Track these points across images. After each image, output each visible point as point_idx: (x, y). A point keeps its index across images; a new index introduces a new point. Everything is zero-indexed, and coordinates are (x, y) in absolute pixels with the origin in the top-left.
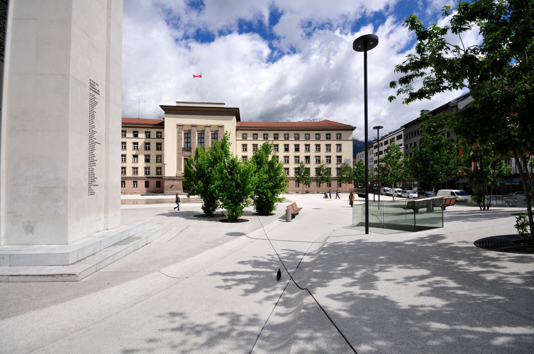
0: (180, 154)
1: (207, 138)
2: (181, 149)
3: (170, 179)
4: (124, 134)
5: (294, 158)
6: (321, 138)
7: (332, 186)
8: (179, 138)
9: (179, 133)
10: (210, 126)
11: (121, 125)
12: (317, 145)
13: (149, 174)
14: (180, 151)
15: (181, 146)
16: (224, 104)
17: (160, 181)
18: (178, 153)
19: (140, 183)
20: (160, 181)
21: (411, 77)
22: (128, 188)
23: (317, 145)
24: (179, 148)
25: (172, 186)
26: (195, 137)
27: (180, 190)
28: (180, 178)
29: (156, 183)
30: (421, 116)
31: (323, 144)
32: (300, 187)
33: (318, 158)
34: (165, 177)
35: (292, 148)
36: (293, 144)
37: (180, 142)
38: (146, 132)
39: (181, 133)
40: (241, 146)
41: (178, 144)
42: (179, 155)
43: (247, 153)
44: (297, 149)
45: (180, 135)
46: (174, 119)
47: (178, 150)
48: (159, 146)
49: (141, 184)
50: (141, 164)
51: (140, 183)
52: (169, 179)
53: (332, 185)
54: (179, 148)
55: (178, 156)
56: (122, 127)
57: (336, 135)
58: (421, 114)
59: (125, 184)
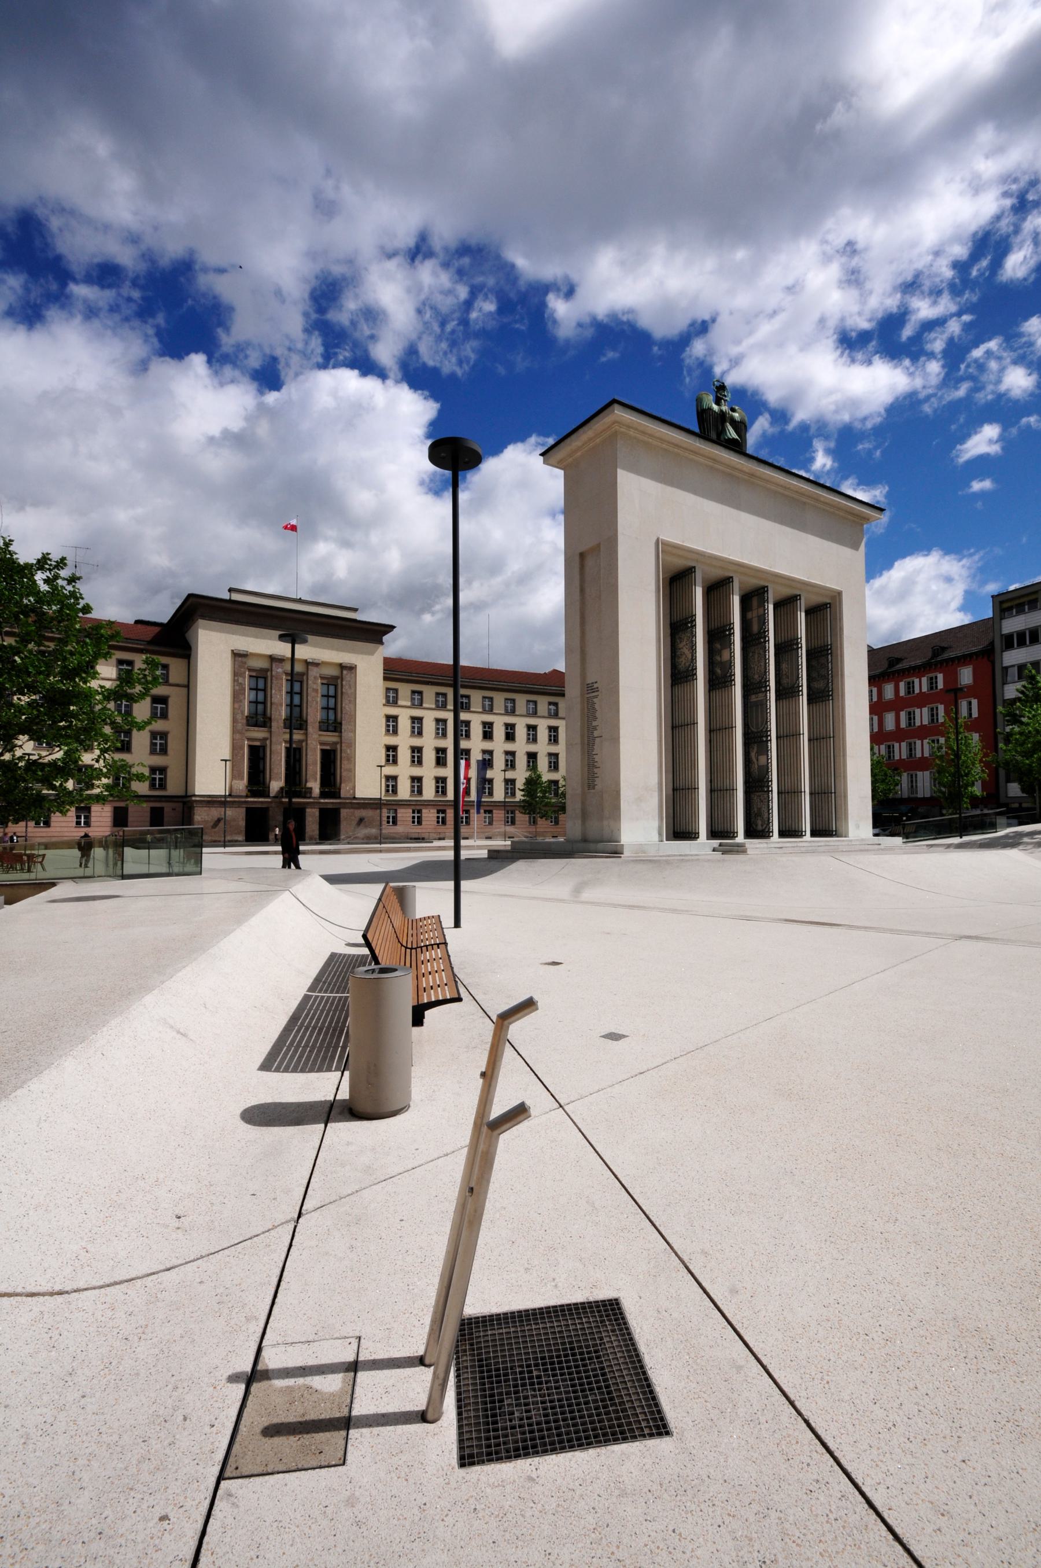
0: (241, 733)
1: (314, 694)
2: (242, 719)
3: (212, 801)
4: (392, 698)
5: (503, 755)
6: (494, 708)
7: (423, 823)
8: (237, 688)
9: (236, 674)
10: (316, 665)
11: (382, 671)
12: (414, 719)
13: (163, 786)
14: (239, 726)
15: (243, 712)
16: (355, 610)
17: (162, 809)
18: (234, 731)
19: (98, 814)
20: (162, 809)
21: (932, 658)
22: (58, 829)
23: (414, 719)
24: (239, 717)
25: (219, 820)
26: (281, 690)
27: (239, 833)
28: (243, 800)
29: (148, 814)
30: (35, 562)
31: (429, 719)
32: (447, 826)
33: (487, 757)
34: (195, 796)
35: (499, 732)
36: (432, 718)
37: (241, 701)
38: (120, 662)
39: (243, 675)
40: (384, 720)
41: (236, 706)
42: (238, 736)
43: (398, 737)
44: (510, 736)
45: (241, 680)
46: (223, 636)
47: (234, 721)
48: (159, 706)
49: (429, 816)
50: (429, 771)
51: (98, 814)
52: (209, 802)
53: (423, 819)
54: (239, 717)
55: (233, 740)
56: (385, 679)
57: (434, 696)
58: (38, 560)
59: (87, 818)
